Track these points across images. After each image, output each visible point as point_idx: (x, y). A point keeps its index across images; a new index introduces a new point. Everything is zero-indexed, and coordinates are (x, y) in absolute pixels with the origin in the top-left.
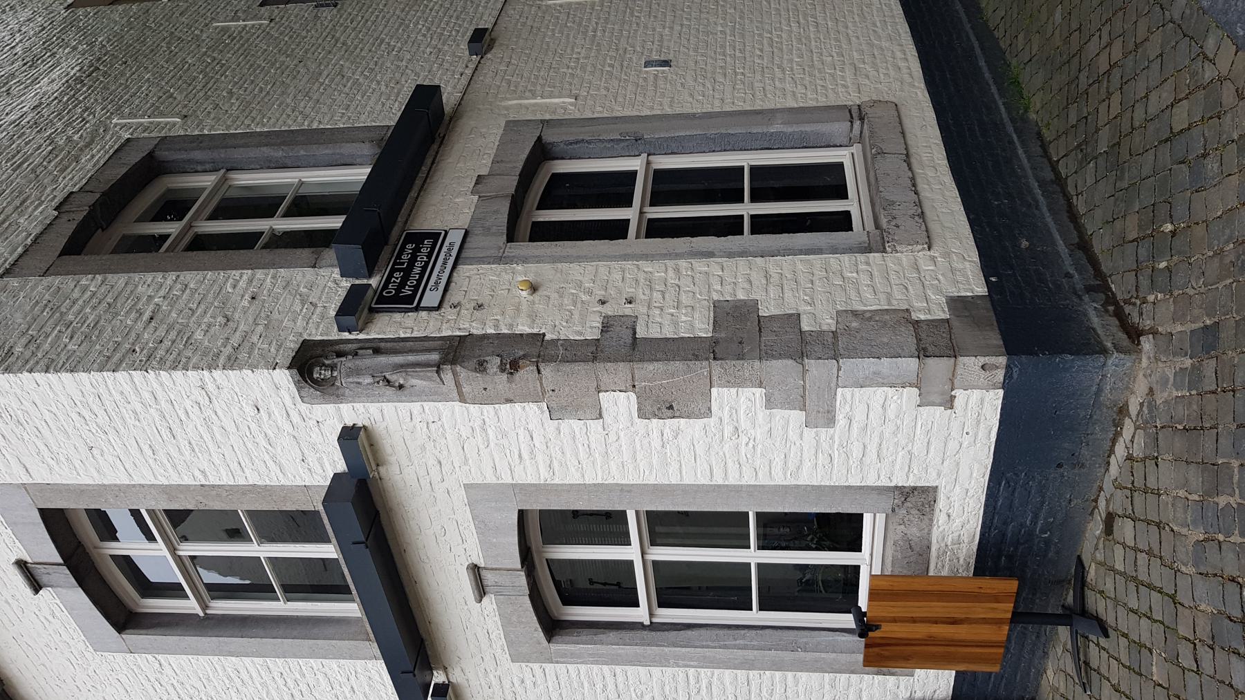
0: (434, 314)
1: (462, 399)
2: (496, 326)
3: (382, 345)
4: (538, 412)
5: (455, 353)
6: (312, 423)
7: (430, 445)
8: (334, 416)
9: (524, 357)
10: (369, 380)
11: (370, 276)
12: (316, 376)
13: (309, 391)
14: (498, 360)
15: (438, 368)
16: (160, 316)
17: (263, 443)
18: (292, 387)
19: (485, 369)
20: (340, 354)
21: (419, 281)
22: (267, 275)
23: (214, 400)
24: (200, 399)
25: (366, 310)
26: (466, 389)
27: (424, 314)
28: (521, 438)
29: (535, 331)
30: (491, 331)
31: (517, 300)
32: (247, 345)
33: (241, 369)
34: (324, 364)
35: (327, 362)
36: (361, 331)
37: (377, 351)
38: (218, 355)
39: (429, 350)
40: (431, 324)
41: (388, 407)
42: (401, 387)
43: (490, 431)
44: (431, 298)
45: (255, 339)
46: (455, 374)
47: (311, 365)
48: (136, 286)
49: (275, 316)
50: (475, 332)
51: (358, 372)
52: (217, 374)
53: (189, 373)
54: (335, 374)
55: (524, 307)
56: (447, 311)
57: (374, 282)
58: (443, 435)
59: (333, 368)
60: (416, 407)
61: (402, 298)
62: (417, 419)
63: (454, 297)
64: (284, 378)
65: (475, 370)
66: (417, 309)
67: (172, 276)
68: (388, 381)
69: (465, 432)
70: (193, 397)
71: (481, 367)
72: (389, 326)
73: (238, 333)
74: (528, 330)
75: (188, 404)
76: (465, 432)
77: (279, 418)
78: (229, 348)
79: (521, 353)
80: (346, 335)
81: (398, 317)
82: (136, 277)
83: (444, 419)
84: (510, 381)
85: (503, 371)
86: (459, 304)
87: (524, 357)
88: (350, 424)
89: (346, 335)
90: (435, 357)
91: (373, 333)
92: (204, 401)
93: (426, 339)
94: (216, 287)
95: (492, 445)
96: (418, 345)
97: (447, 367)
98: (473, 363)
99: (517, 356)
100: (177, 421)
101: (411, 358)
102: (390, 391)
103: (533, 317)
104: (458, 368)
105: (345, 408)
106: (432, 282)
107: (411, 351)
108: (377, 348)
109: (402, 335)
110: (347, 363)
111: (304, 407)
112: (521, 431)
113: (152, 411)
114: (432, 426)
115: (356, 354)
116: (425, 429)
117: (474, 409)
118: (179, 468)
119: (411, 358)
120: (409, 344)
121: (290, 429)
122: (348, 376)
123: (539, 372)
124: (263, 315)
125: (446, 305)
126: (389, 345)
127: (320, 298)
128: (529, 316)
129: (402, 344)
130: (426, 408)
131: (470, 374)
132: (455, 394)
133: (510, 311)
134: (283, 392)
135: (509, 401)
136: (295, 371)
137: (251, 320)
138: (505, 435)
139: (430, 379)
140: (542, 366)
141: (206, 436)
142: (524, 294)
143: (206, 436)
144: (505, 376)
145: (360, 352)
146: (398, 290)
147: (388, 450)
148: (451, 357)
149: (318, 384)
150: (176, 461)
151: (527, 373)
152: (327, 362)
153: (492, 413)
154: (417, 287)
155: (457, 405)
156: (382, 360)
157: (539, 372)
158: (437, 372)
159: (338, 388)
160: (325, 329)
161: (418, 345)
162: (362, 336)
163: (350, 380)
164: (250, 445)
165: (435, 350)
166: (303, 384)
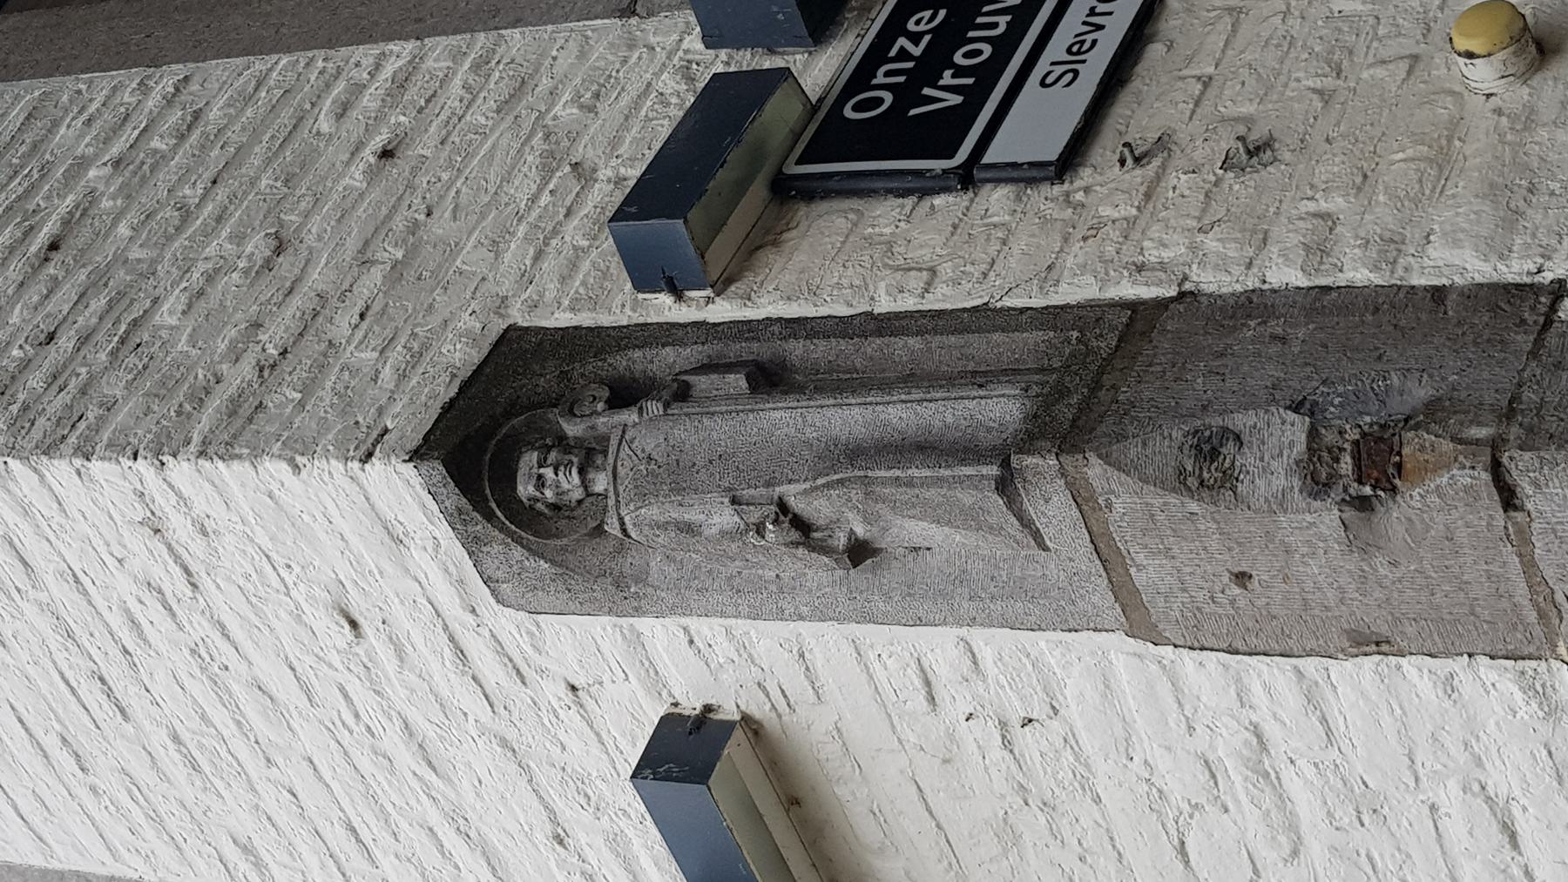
0: (1044, 198)
1: (1139, 621)
2: (1318, 251)
3: (796, 349)
4: (1528, 710)
5: (1095, 387)
6: (554, 692)
7: (1032, 824)
8: (640, 662)
9: (1432, 413)
10: (723, 518)
11: (819, 31)
12: (525, 490)
13: (506, 554)
14: (1293, 432)
15: (1003, 463)
16: (84, 234)
17: (406, 759)
18: (444, 532)
19: (1229, 479)
20: (624, 394)
21: (1004, 46)
22: (457, 56)
23: (205, 582)
24: (157, 573)
25: (758, 191)
26: (1148, 573)
27: (997, 199)
28: (1455, 829)
29: (1515, 270)
30: (1286, 274)
31: (1444, 109)
32: (313, 346)
33: (256, 454)
34: (562, 442)
35: (573, 429)
36: (721, 286)
37: (770, 379)
38: (199, 398)
39: (981, 378)
40: (1018, 245)
41: (828, 642)
42: (859, 552)
43: (1293, 784)
44: (1037, 122)
45: (342, 324)
46: (1082, 498)
47: (511, 446)
48: (56, 124)
49: (442, 226)
50: (1209, 281)
51: (674, 477)
52: (181, 470)
53: (97, 467)
54: (601, 483)
55: (1477, 148)
56: (1105, 184)
57: (819, 69)
58: (1086, 786)
59: (589, 455)
60: (940, 645)
61: (909, 134)
62: (956, 701)
63: (1135, 117)
64: (404, 493)
65: (1180, 482)
66: (967, 178)
67: (166, 80)
68: (802, 526)
69: (1182, 782)
70: (134, 564)
71: (1209, 465)
72: (859, 260)
73: (296, 301)
74: (1475, 267)
75: (125, 587)
76: (1182, 782)
77: (435, 666)
78: (247, 368)
79: (1421, 392)
80: (663, 308)
81: (886, 215)
82: (67, 86)
83: (1072, 711)
84: (1359, 542)
85: (1317, 484)
86: (1163, 143)
87: (1432, 413)
88: (691, 705)
89: (663, 308)
90: (1002, 409)
91: (766, 300)
92: (174, 584)
93: (983, 318)
94: (286, 116)
95: (1315, 848)
96: (945, 349)
97: (1039, 465)
98: (1167, 445)
99: (1399, 406)
100: (115, 652)
101: (899, 415)
102: (818, 572)
103: (1512, 197)
104: (1095, 471)
105: (660, 633)
106: (1056, 48)
107: (914, 380)
108: (770, 367)
109: (885, 304)
110: (644, 433)
111: (507, 622)
112: (1450, 796)
113: (30, 610)
114: (1026, 739)
115: (683, 394)
116: (997, 753)
117: (1203, 672)
118: (172, 824)
119: (899, 415)
120: (906, 347)
121: (479, 708)
122: (642, 496)
123: (1509, 498)
124: (399, 223)
125: (1104, 150)
126: (820, 350)
127: (615, 143)
128: (1493, 191)
129: (873, 345)
130: (986, 655)
131: (1156, 499)
132: (1100, 596)
133: (1399, 163)
134: (420, 558)
135: (1368, 642)
136: (437, 470)
137: (352, 244)
138: (1369, 807)
139: (972, 519)
140: (1521, 466)
141: (219, 716)
142: (1483, 74)
143: (219, 716)
144: (1327, 518)
145: (701, 383)
146: (907, 94)
147: (867, 831)
148: (1065, 412)
149: (532, 524)
150: (156, 799)
151: (1442, 501)
152: (573, 429)
153: (1292, 699)
154: (987, 74)
155: (1119, 648)
156: (783, 420)
157: (1509, 498)
158: (1005, 485)
159: (621, 549)
160: (583, 288)
161: (945, 349)
162: (723, 310)
163: (652, 512)
164: (365, 764)
165: (1009, 373)
166: (480, 527)
